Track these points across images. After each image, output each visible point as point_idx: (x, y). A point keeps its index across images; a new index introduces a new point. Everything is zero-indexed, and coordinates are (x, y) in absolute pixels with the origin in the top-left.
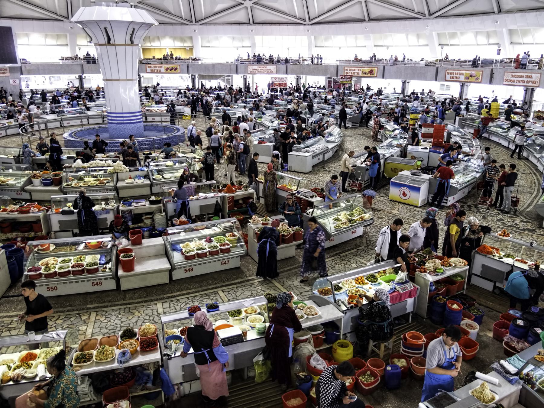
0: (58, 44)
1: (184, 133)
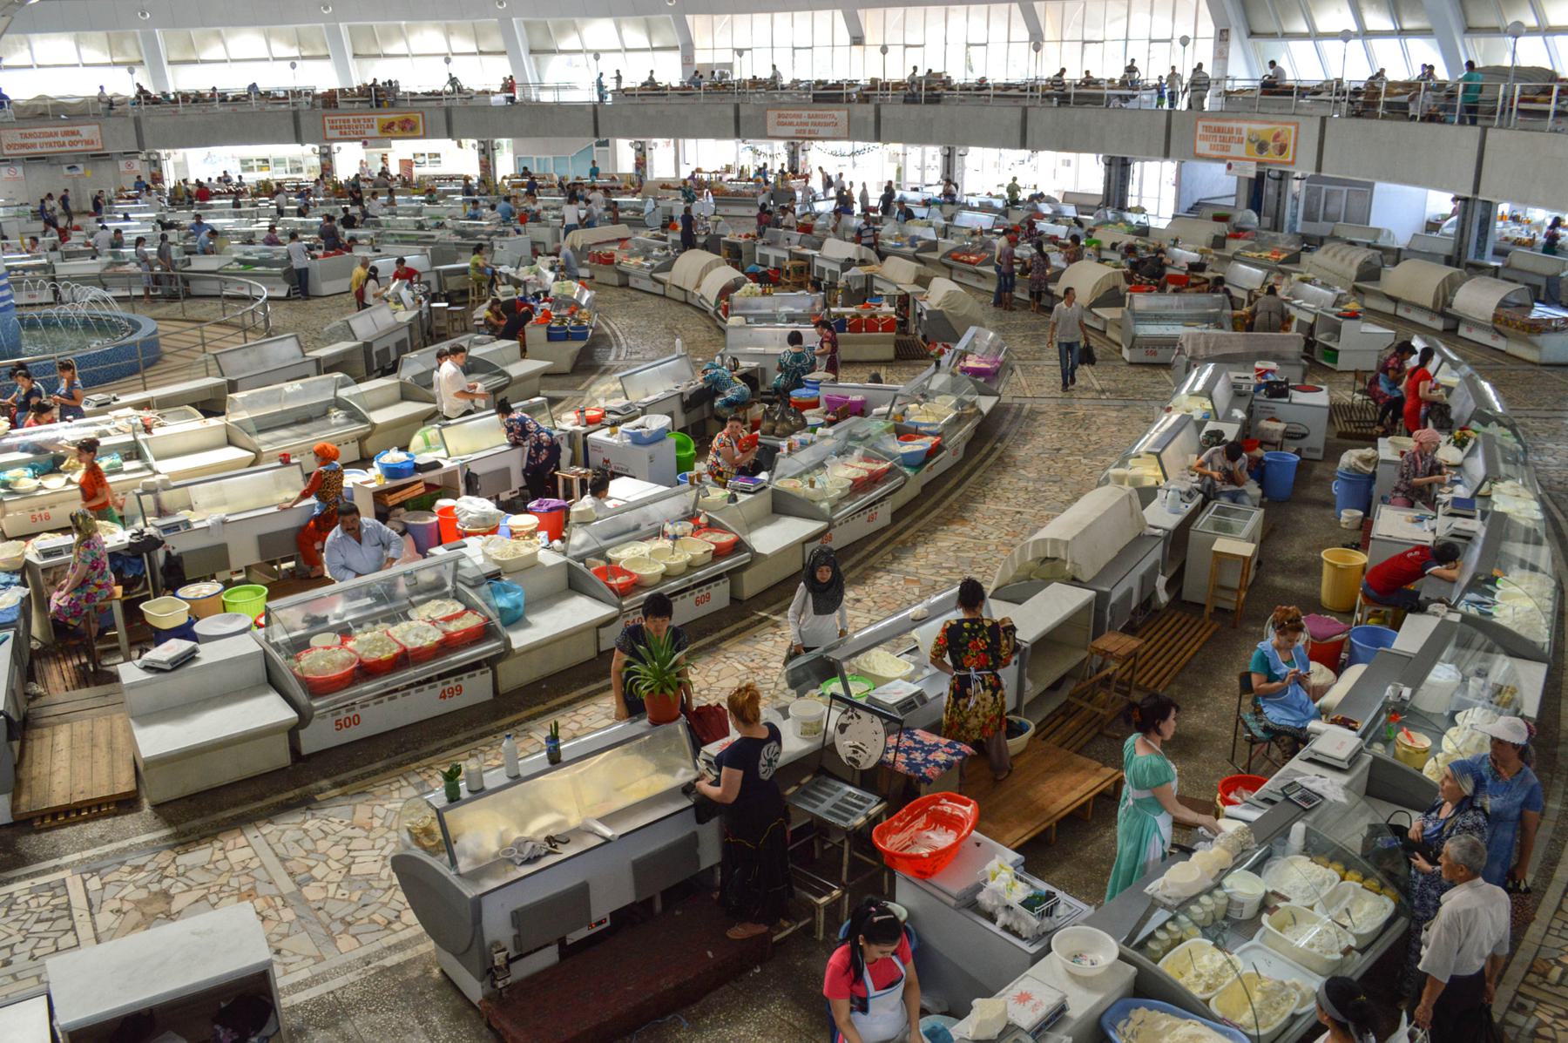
0: (115, 60)
1: (155, 332)
